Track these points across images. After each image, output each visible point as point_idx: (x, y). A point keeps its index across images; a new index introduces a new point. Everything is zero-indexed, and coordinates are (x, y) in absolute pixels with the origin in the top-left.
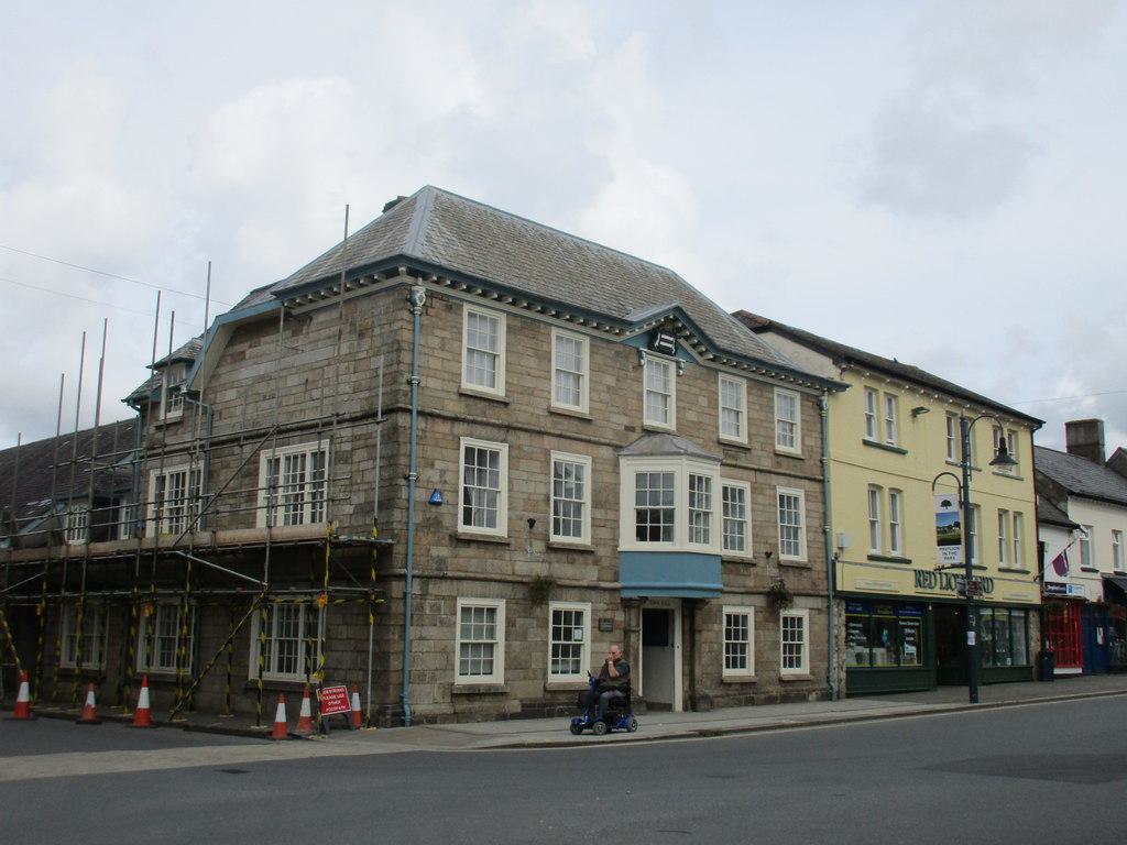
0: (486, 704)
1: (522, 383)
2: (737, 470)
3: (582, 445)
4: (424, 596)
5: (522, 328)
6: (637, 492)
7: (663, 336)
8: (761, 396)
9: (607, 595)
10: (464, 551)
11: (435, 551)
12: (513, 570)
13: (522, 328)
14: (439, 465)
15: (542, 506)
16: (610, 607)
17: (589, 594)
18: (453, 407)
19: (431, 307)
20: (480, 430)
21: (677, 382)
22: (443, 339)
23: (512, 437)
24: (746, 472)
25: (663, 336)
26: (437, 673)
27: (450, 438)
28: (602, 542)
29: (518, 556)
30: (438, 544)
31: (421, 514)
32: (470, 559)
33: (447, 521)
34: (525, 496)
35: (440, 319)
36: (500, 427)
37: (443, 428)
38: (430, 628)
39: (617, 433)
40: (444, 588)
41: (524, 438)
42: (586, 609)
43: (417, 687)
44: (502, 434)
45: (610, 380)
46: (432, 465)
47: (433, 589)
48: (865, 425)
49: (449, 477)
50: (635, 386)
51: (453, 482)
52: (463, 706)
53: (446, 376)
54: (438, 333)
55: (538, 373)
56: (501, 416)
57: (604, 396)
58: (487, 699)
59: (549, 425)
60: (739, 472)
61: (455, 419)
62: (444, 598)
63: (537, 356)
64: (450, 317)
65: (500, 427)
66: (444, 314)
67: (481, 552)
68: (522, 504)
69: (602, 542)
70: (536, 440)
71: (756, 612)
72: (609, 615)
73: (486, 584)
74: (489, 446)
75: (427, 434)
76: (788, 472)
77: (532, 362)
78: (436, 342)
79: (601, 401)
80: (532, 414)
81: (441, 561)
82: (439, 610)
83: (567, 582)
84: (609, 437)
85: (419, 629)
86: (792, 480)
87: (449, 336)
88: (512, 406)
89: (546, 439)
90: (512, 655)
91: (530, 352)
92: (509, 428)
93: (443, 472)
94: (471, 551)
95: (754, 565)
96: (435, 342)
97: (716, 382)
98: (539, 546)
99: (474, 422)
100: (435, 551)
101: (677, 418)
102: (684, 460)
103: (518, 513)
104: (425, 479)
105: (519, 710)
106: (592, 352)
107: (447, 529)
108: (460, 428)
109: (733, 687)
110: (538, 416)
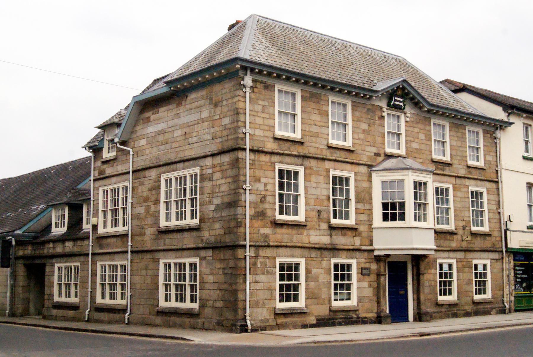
3: (348, 166)
4: (257, 257)
7: (396, 98)
10: (279, 230)
12: (309, 240)
14: (263, 180)
15: (326, 203)
18: (271, 146)
19: (256, 87)
22: (263, 106)
23: (306, 162)
25: (396, 98)
26: (266, 302)
29: (312, 232)
30: (264, 226)
33: (269, 213)
36: (298, 156)
37: (265, 158)
39: (369, 158)
40: (268, 252)
42: (354, 262)
44: (300, 161)
45: (364, 126)
46: (259, 180)
47: (263, 253)
49: (269, 187)
50: (380, 129)
51: (272, 190)
53: (267, 128)
54: (260, 102)
57: (362, 136)
61: (272, 153)
62: (268, 258)
64: (268, 93)
65: (298, 156)
70: (321, 164)
71: (457, 262)
72: (367, 265)
75: (256, 163)
77: (316, 117)
79: (359, 139)
81: (266, 236)
82: (266, 265)
85: (254, 276)
87: (267, 104)
90: (310, 290)
91: (316, 112)
93: (266, 185)
94: (284, 230)
98: (324, 226)
102: (410, 173)
103: (311, 207)
104: (256, 188)
107: (269, 217)
109: (444, 307)
110: (322, 149)
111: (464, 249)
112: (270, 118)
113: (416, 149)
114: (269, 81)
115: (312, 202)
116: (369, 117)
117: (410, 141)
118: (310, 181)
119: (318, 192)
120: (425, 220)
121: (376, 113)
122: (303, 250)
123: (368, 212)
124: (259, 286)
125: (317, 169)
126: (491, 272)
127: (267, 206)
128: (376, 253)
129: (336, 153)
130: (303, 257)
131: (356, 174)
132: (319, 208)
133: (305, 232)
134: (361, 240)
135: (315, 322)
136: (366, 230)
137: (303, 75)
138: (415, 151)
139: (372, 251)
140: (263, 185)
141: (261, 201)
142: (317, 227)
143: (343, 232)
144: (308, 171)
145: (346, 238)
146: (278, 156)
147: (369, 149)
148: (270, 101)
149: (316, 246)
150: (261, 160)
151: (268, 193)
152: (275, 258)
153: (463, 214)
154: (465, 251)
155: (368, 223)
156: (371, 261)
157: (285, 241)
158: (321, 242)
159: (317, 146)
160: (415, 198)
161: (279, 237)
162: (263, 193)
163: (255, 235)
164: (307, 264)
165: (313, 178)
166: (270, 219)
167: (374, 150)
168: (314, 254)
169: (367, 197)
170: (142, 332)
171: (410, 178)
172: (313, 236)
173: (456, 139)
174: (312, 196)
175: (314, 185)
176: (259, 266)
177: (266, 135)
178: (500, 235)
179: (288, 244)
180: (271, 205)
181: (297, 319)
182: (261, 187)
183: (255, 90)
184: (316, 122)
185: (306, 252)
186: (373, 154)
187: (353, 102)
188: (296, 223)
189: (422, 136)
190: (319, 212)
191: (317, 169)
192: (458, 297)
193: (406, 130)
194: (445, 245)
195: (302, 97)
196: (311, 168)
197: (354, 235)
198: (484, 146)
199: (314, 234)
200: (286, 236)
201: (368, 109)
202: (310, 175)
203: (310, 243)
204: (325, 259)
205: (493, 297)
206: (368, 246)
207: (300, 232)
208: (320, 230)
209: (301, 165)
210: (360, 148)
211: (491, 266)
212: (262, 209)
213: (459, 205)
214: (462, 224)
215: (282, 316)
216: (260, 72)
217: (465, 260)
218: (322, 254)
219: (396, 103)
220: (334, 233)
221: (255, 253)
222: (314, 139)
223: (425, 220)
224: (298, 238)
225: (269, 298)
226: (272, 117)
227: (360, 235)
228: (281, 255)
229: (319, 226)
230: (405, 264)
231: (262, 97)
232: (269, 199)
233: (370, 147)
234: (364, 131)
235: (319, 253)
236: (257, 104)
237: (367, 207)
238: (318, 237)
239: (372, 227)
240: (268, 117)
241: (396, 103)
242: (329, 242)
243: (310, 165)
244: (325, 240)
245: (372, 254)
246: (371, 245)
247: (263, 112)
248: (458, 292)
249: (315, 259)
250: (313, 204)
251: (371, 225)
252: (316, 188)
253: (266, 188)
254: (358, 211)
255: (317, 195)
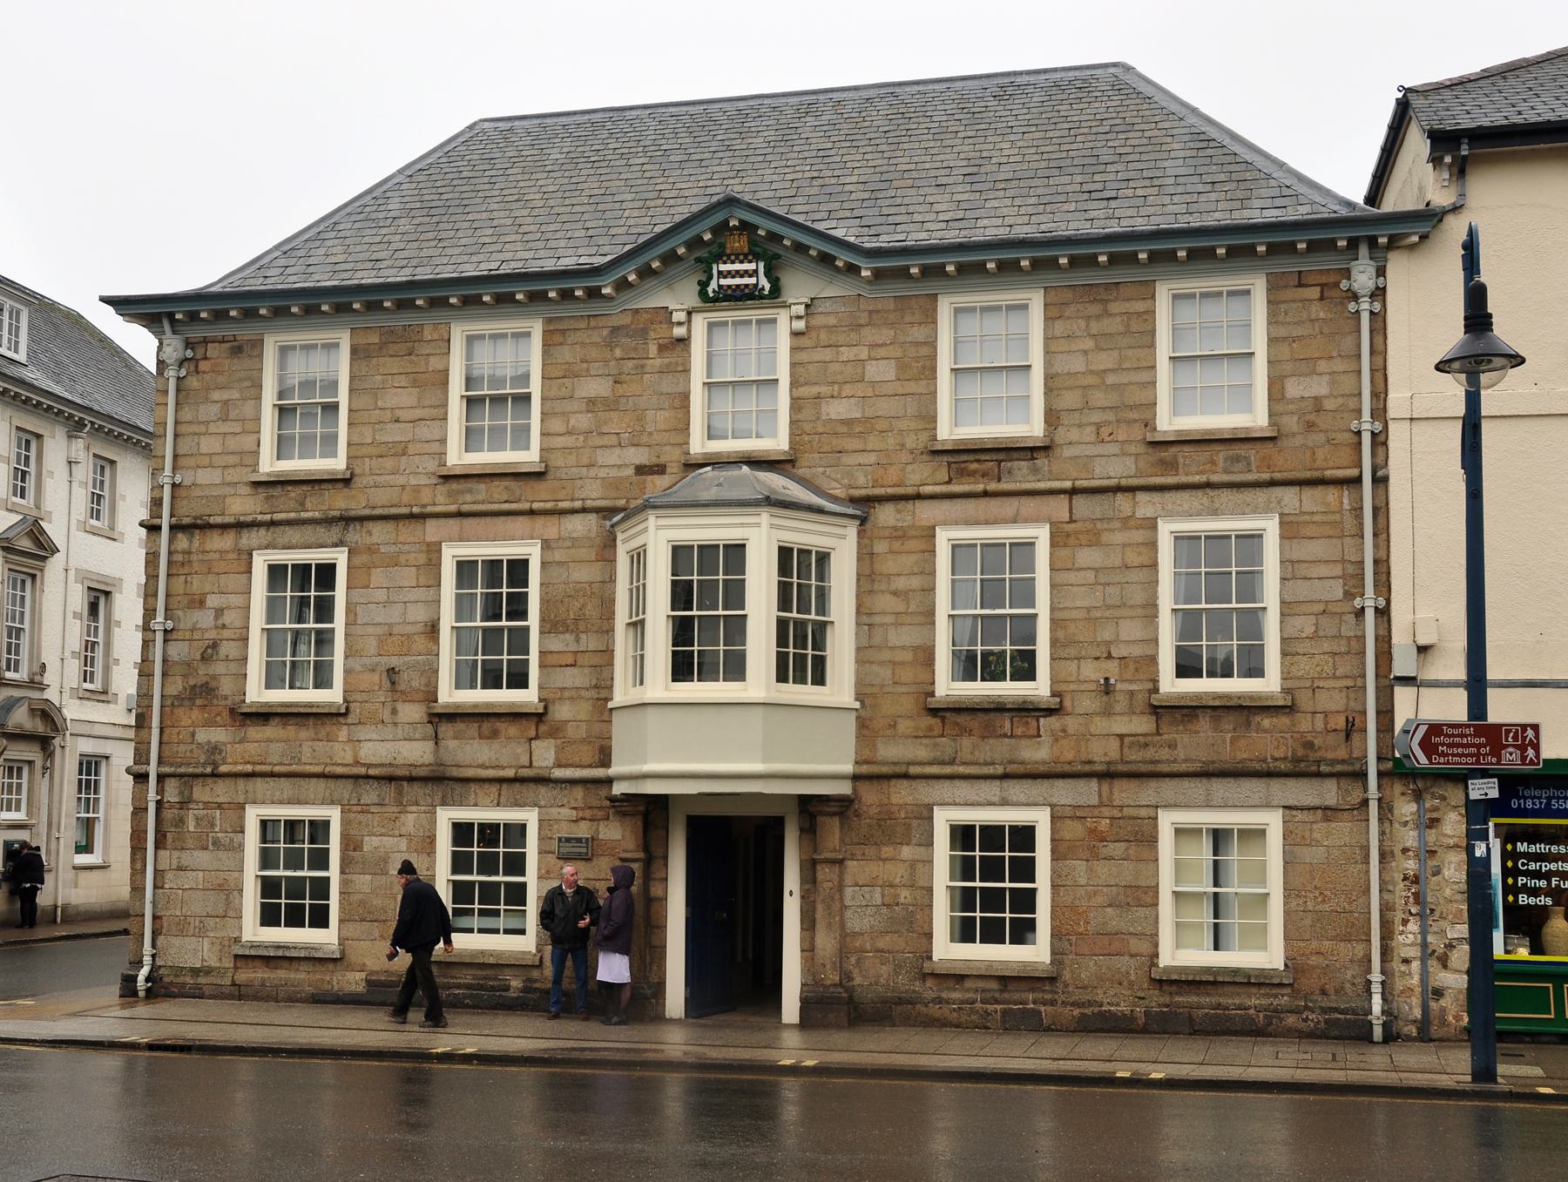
0: (300, 977)
1: (380, 437)
2: (1319, 492)
3: (521, 523)
4: (184, 804)
5: (383, 345)
6: (673, 582)
7: (723, 267)
8: (1107, 314)
9: (579, 792)
10: (255, 732)
11: (203, 736)
12: (355, 756)
13: (383, 345)
14: (213, 601)
15: (421, 643)
16: (588, 814)
17: (530, 791)
18: (243, 505)
19: (205, 358)
20: (292, 534)
21: (793, 349)
22: (226, 402)
23: (355, 535)
24: (1029, 505)
25: (723, 267)
26: (211, 922)
27: (234, 556)
28: (567, 694)
29: (363, 733)
30: (209, 723)
31: (179, 680)
32: (267, 744)
33: (226, 687)
34: (379, 630)
35: (221, 373)
36: (328, 521)
37: (219, 542)
38: (197, 853)
39: (614, 484)
40: (222, 791)
41: (379, 533)
42: (530, 817)
43: (176, 941)
44: (335, 532)
45: (596, 387)
46: (202, 603)
47: (200, 792)
48: (1495, 305)
49: (229, 618)
50: (668, 384)
51: (238, 624)
52: (257, 975)
53: (232, 460)
54: (216, 395)
55: (419, 413)
56: (338, 502)
57: (582, 421)
58: (304, 967)
59: (440, 499)
60: (1009, 506)
61: (240, 526)
62: (219, 806)
63: (415, 384)
64: (239, 364)
65: (328, 521)
66: (227, 362)
67: (291, 731)
68: (375, 643)
69: (567, 694)
70: (408, 532)
71: (1054, 819)
72: (583, 830)
73: (301, 781)
74: (505, 550)
75: (194, 557)
76: (1197, 479)
77: (402, 398)
78: (213, 410)
79: (569, 433)
80: (403, 487)
81: (214, 749)
82: (213, 825)
83: (470, 773)
84: (593, 493)
85: (176, 854)
86: (1226, 496)
87: (236, 395)
88: (358, 482)
89: (431, 525)
90: (355, 898)
91: (403, 380)
92: (347, 520)
93: (219, 612)
94: (271, 731)
95: (1050, 712)
96: (210, 411)
97: (931, 318)
98: (412, 712)
99: (273, 523)
100: (203, 736)
101: (793, 423)
102: (764, 517)
103: (367, 661)
104: (189, 626)
105: (361, 988)
106: (1048, 319)
107: (226, 698)
108: (249, 538)
109: (968, 984)
110: (417, 489)
111: (1098, 768)
112: (244, 432)
113: (848, 422)
114: (245, 333)
115: (371, 645)
116: (618, 353)
117: (818, 397)
118: (367, 587)
119: (394, 614)
120: (820, 680)
121: (652, 335)
122: (331, 783)
123: (596, 660)
124: (188, 880)
125: (393, 548)
126: (1288, 863)
127: (219, 668)
128: (618, 789)
129: (470, 491)
130: (332, 803)
131: (546, 545)
132: (394, 662)
133: (343, 734)
134: (559, 750)
135: (361, 988)
136: (583, 716)
137: (360, 289)
138: (843, 429)
139: (609, 781)
140: (212, 614)
141: (204, 658)
142: (387, 717)
143: (486, 726)
144: (359, 560)
145: (496, 745)
146: (263, 531)
147: (611, 457)
148: (248, 383)
149: (372, 772)
150: (208, 548)
151: (226, 634)
152: (241, 807)
153: (1106, 634)
154: (1108, 775)
155: (593, 694)
156: (600, 814)
157: (275, 759)
158: (400, 761)
159: (401, 480)
160: (784, 604)
161: (253, 749)
162: (212, 635)
163: (182, 748)
164: (345, 823)
165: (378, 577)
166: (229, 702)
167: (641, 456)
168: (370, 794)
169: (592, 611)
170: (98, 930)
171: (761, 539)
172: (370, 744)
173: (1089, 344)
174: (370, 630)
175: (381, 595)
176: (191, 829)
177: (229, 479)
178: (161, 940)
179: (277, 769)
180: (233, 667)
181: (302, 976)
182: (205, 619)
183: (203, 365)
184: (399, 413)
185: (344, 789)
186: (630, 471)
187: (548, 321)
188: (302, 710)
189: (882, 371)
190: (391, 671)
191: (393, 548)
192: (1054, 952)
193: (793, 365)
194: (980, 756)
195: (354, 351)
196: (371, 550)
197: (533, 733)
198: (1272, 341)
199: (374, 736)
200: (276, 748)
201: (615, 330)
202: (369, 568)
203: (357, 763)
204: (414, 808)
205: (1290, 962)
206: (590, 766)
207: (323, 733)
208: (395, 724)
209: (336, 545)
210: (572, 460)
211: (1286, 835)
212: (205, 679)
213: (1081, 599)
214: (1092, 672)
215: (258, 963)
216: (193, 317)
217: (1106, 812)
218: (400, 793)
219: (723, 282)
220: (445, 729)
221: (181, 793)
222: (389, 463)
223: (820, 680)
224: (312, 750)
225: (221, 912)
226: (250, 426)
227: (556, 732)
228: (260, 797)
229: (394, 712)
230: (777, 824)
231: (221, 379)
232: (228, 649)
233: (617, 451)
234: (591, 403)
235: (389, 791)
236: (207, 400)
237: (590, 642)
238: (389, 745)
239: (610, 705)
240: (238, 430)
241: (723, 282)
242: (428, 758)
243: (368, 540)
244: (417, 753)
245: (603, 793)
246: (606, 763)
247: (225, 419)
248: (1056, 934)
249: (373, 809)
250: (373, 651)
251: (607, 700)
252: (388, 603)
253: (220, 622)
254: (550, 660)
255: (391, 625)
